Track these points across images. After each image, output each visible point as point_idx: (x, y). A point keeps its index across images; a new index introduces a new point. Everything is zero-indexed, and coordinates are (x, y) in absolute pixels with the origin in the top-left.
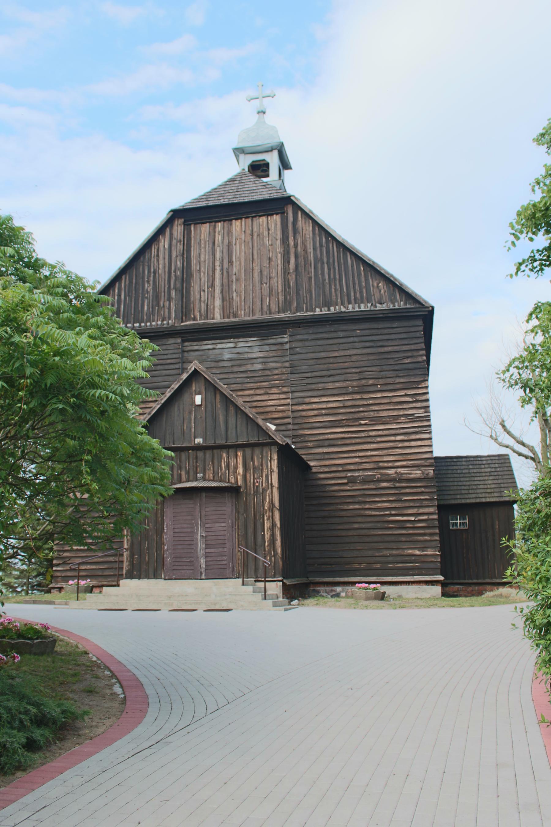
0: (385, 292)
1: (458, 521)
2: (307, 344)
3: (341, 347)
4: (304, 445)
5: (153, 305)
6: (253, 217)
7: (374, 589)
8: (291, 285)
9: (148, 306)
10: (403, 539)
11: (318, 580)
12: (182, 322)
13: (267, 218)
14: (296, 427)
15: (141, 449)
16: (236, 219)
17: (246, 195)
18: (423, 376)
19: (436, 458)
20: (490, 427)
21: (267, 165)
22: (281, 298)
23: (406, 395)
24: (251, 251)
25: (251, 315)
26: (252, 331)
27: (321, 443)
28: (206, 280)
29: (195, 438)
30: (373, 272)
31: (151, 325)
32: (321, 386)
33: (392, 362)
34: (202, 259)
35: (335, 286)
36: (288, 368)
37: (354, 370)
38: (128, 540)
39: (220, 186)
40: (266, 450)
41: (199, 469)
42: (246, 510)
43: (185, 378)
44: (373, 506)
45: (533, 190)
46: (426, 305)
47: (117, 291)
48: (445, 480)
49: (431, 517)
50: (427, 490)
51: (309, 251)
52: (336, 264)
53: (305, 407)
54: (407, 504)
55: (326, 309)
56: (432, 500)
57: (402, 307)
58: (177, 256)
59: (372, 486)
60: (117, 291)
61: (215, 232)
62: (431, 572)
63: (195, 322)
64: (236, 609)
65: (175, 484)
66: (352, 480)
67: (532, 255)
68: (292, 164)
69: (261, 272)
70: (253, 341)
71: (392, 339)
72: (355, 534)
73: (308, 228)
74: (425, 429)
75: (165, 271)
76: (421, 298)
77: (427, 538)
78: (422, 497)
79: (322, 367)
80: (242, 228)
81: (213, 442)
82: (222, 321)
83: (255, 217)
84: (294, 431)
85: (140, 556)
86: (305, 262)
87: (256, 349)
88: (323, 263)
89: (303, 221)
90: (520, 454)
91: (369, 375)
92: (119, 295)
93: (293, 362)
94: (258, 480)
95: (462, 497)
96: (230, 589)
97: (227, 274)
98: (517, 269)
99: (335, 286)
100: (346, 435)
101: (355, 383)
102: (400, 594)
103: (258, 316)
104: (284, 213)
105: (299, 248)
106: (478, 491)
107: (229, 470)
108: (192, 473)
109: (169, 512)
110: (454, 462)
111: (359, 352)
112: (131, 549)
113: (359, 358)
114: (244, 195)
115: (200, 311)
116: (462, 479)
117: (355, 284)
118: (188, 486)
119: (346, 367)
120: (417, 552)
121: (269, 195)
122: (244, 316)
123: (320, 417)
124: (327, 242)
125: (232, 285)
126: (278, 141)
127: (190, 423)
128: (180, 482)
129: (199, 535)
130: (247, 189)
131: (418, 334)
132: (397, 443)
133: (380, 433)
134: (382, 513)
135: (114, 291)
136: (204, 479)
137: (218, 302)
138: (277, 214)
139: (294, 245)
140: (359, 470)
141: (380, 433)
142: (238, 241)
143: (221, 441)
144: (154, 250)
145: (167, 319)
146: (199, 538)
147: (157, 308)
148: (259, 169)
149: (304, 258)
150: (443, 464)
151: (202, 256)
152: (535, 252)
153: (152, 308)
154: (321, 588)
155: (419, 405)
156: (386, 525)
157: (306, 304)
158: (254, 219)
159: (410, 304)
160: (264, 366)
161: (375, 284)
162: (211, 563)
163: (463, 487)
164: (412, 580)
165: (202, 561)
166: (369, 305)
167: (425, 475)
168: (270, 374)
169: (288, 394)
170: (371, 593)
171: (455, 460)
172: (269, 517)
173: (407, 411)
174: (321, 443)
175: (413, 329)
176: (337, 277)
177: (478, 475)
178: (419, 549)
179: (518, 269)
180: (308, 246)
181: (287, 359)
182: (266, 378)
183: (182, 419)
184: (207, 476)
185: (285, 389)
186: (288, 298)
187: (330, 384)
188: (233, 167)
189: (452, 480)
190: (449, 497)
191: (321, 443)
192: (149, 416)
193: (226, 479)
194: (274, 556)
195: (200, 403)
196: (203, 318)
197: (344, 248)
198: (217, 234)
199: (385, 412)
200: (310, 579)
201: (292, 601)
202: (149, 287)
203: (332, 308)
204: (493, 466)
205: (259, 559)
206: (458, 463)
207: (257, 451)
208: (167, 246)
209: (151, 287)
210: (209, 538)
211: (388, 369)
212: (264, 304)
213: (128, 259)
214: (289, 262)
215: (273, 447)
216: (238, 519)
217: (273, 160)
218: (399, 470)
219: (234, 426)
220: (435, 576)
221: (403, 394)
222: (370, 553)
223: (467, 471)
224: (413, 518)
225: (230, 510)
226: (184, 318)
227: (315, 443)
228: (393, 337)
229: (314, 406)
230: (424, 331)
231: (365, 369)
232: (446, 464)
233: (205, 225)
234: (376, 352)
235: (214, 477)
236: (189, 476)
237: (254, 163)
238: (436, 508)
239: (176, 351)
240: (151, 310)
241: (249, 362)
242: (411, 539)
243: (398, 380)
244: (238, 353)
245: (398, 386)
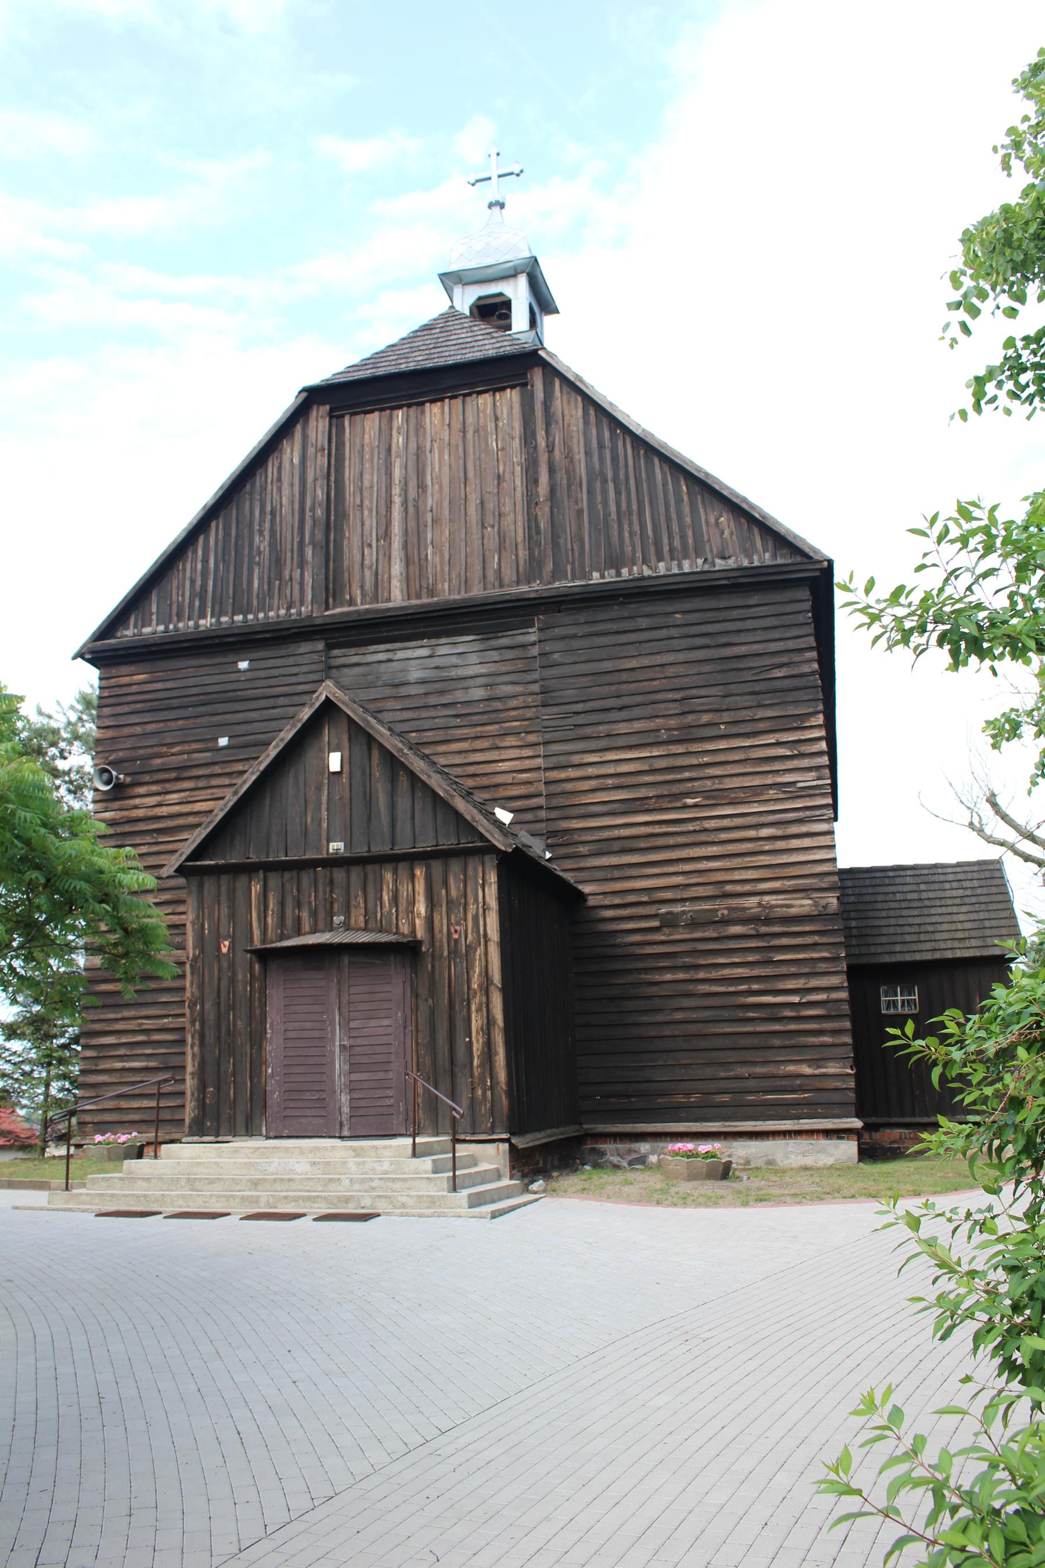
0: (731, 534)
1: (899, 998)
2: (576, 644)
3: (645, 648)
4: (571, 850)
5: (269, 577)
6: (465, 395)
7: (708, 1155)
8: (542, 526)
9: (261, 579)
10: (777, 1042)
11: (601, 1128)
12: (327, 609)
13: (494, 395)
14: (553, 814)
15: (66, 873)
16: (432, 402)
17: (452, 353)
18: (813, 703)
19: (842, 872)
20: (968, 808)
21: (507, 304)
22: (523, 554)
23: (778, 744)
24: (461, 462)
25: (463, 592)
26: (464, 623)
27: (606, 846)
28: (375, 525)
29: (328, 841)
30: (707, 496)
31: (266, 617)
32: (603, 729)
33: (748, 676)
34: (366, 483)
35: (630, 525)
36: (537, 694)
37: (670, 696)
38: (194, 1055)
39: (403, 339)
40: (473, 863)
41: (336, 906)
42: (432, 992)
43: (306, 717)
44: (714, 974)
45: (1006, 166)
46: (816, 557)
47: (200, 552)
48: (871, 914)
49: (834, 995)
50: (825, 940)
51: (577, 457)
52: (632, 481)
53: (571, 773)
54: (783, 970)
55: (613, 572)
56: (835, 959)
57: (768, 562)
58: (315, 480)
59: (710, 933)
60: (200, 552)
61: (391, 429)
62: (836, 1111)
63: (351, 609)
64: (387, 1214)
65: (288, 938)
66: (669, 922)
67: (1011, 352)
68: (559, 298)
69: (482, 503)
70: (466, 643)
71: (748, 630)
72: (677, 1033)
73: (574, 413)
74: (818, 813)
75: (293, 510)
76: (807, 543)
77: (827, 1039)
78: (816, 955)
79: (606, 690)
80: (443, 418)
81: (366, 849)
82: (405, 604)
83: (470, 394)
84: (550, 823)
85: (218, 1088)
86: (569, 480)
87: (474, 658)
88: (605, 481)
89: (565, 398)
90: (1027, 858)
91: (702, 704)
92: (205, 561)
93: (546, 683)
94: (458, 928)
95: (905, 948)
96: (388, 1162)
97: (414, 510)
98: (974, 395)
99: (630, 525)
100: (657, 829)
101: (673, 722)
102: (770, 1157)
103: (477, 592)
104: (525, 385)
105: (557, 453)
106: (938, 936)
107: (397, 906)
108: (321, 914)
109: (276, 997)
110: (889, 877)
111: (681, 657)
112: (201, 1074)
113: (681, 670)
114: (447, 354)
115: (362, 588)
116: (905, 913)
117: (671, 520)
118: (310, 942)
119: (655, 689)
120: (807, 1070)
121: (495, 351)
122: (448, 592)
123: (604, 793)
124: (613, 437)
125: (425, 532)
126: (528, 255)
127: (319, 810)
128: (299, 933)
129: (337, 1043)
130: (454, 342)
131: (801, 619)
132: (762, 843)
133: (726, 823)
134: (732, 989)
135: (195, 552)
136: (347, 926)
137: (397, 568)
138: (512, 387)
139: (548, 446)
140: (683, 900)
141: (726, 823)
142: (436, 446)
143: (381, 848)
144: (271, 468)
145: (298, 604)
146: (337, 1050)
147: (277, 582)
148: (493, 311)
149: (567, 472)
150: (867, 882)
151: (367, 477)
152: (1019, 344)
153: (269, 583)
154: (608, 1147)
155: (805, 763)
156: (741, 1014)
157: (573, 564)
158: (468, 399)
159: (783, 556)
160: (489, 693)
161: (712, 520)
162: (362, 1103)
163: (907, 929)
164: (796, 1128)
165: (343, 1099)
166: (700, 561)
167: (820, 908)
168: (501, 708)
169: (537, 747)
170: (700, 1164)
171: (891, 874)
172: (481, 1004)
173: (780, 776)
174: (605, 846)
175: (790, 608)
176: (635, 507)
177: (938, 903)
178: (810, 1062)
179: (979, 396)
180: (576, 450)
181: (535, 676)
182: (493, 716)
183: (302, 802)
184: (353, 921)
185: (532, 738)
186: (536, 553)
187: (621, 725)
189: (884, 914)
190: (879, 949)
191: (606, 846)
193: (391, 927)
194: (492, 1088)
195: (338, 769)
196: (368, 599)
197: (646, 448)
198: (394, 432)
199: (735, 779)
200: (585, 1126)
201: (532, 1182)
202: (261, 543)
203: (625, 571)
204: (967, 884)
205: (442, 1100)
206: (898, 881)
207: (455, 866)
208: (296, 461)
209: (266, 543)
210: (357, 1050)
211: (740, 691)
212: (488, 567)
213: (220, 488)
214: (536, 482)
215: (487, 858)
216: (415, 1010)
217: (518, 293)
218: (766, 898)
219: (409, 814)
220: (845, 1120)
221: (773, 741)
222: (709, 1072)
223: (915, 896)
224: (796, 999)
225: (400, 991)
226: (331, 600)
227: (594, 847)
228: (749, 624)
229: (590, 771)
230: (815, 610)
231: (694, 692)
232: (874, 882)
233: (371, 416)
234: (716, 656)
235: (366, 922)
236: (316, 922)
237: (482, 303)
238: (845, 977)
239: (314, 667)
240: (266, 587)
241: (460, 686)
242: (793, 1044)
243: (761, 713)
244: (437, 668)
245: (761, 726)
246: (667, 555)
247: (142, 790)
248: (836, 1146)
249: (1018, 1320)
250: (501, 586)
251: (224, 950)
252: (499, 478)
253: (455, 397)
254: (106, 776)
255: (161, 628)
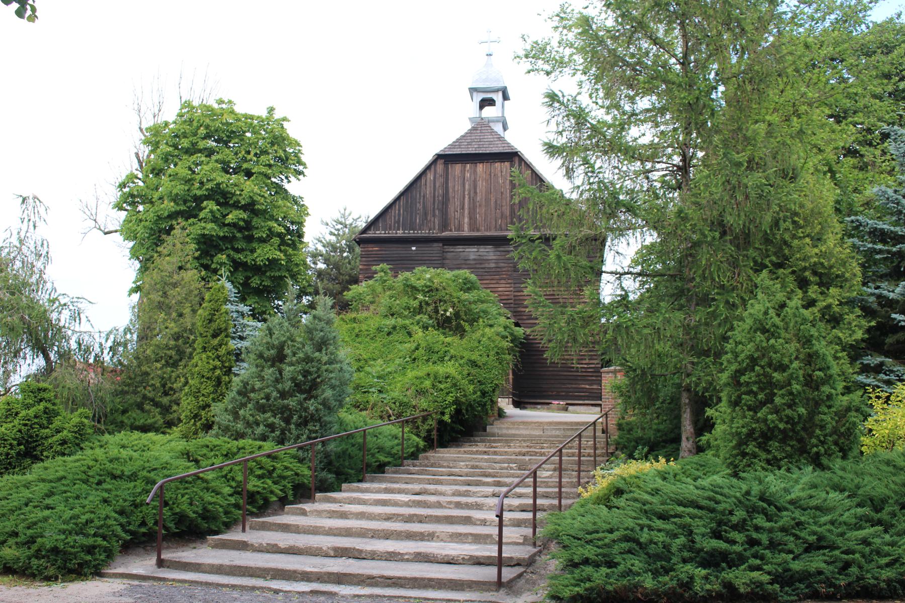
87: (491, 254)
92: (399, 210)
137: (466, 220)
144: (423, 181)
202: (420, 206)
249: (609, 42)
252: (502, 193)
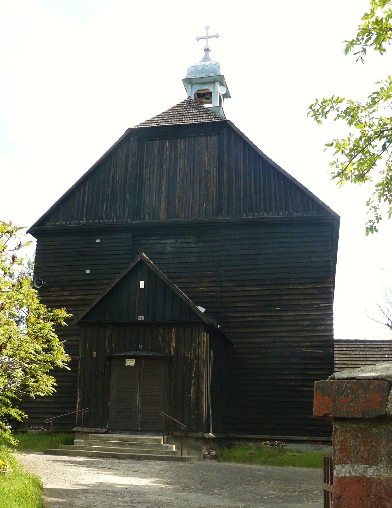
12: (134, 220)
16: (181, 138)
23: (313, 288)
39: (169, 110)
43: (132, 267)
83: (197, 136)
104: (221, 134)
122: (182, 219)
136: (144, 349)
138: (215, 135)
141: (291, 318)
154: (237, 443)
158: (196, 138)
188: (181, 95)
192: (102, 296)
237: (200, 92)
244: (178, 248)
246: (274, 210)
247: (53, 289)
248: (326, 448)
250: (206, 216)
251: (95, 356)
253: (191, 137)
254: (39, 283)
255: (64, 223)
